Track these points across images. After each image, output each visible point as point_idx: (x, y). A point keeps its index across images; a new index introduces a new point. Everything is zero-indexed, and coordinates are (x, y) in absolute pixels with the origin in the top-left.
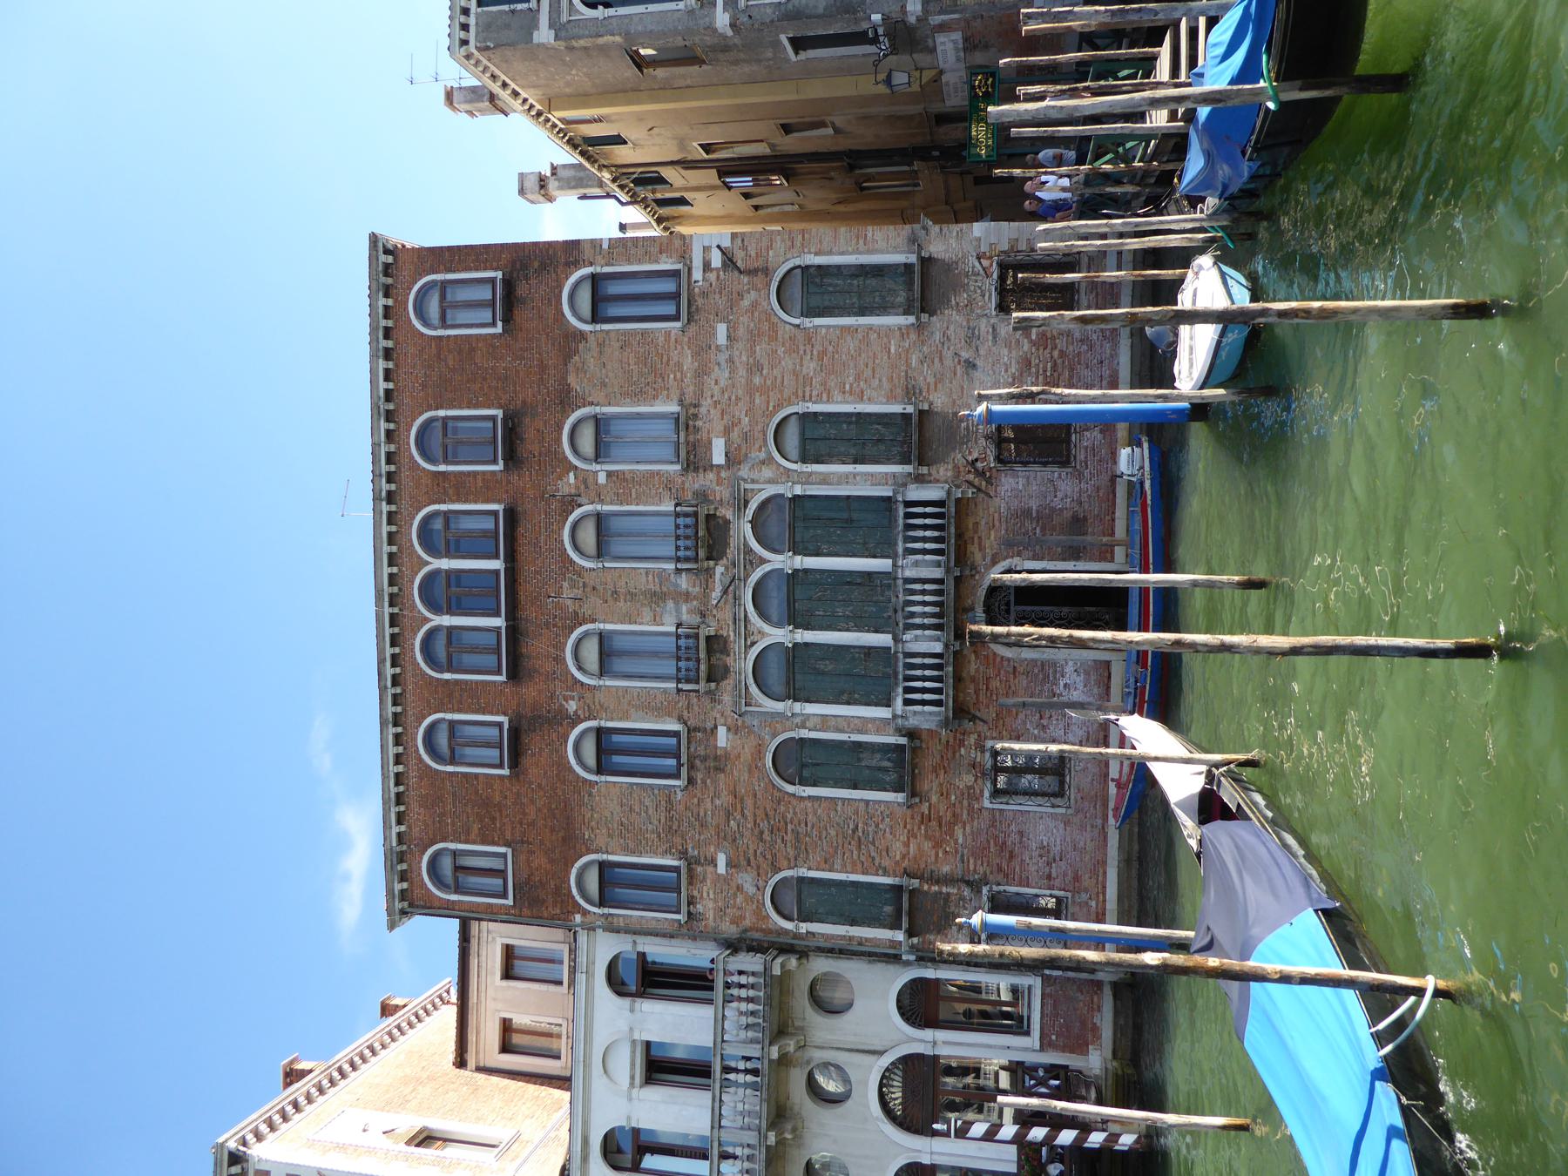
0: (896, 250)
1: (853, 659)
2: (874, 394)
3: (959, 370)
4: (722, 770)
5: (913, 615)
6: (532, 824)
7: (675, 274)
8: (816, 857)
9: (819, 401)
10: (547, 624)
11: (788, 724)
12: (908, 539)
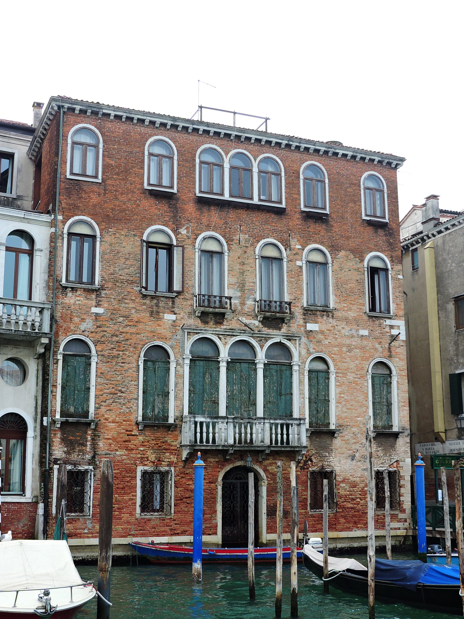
0: (400, 421)
1: (212, 394)
2: (340, 409)
3: (351, 452)
4: (151, 315)
5: (246, 428)
6: (117, 198)
7: (389, 312)
8: (104, 368)
9: (337, 381)
10: (226, 223)
11: (178, 356)
12: (282, 425)
